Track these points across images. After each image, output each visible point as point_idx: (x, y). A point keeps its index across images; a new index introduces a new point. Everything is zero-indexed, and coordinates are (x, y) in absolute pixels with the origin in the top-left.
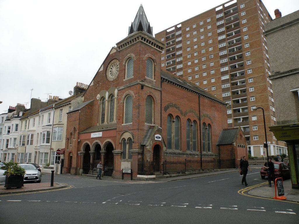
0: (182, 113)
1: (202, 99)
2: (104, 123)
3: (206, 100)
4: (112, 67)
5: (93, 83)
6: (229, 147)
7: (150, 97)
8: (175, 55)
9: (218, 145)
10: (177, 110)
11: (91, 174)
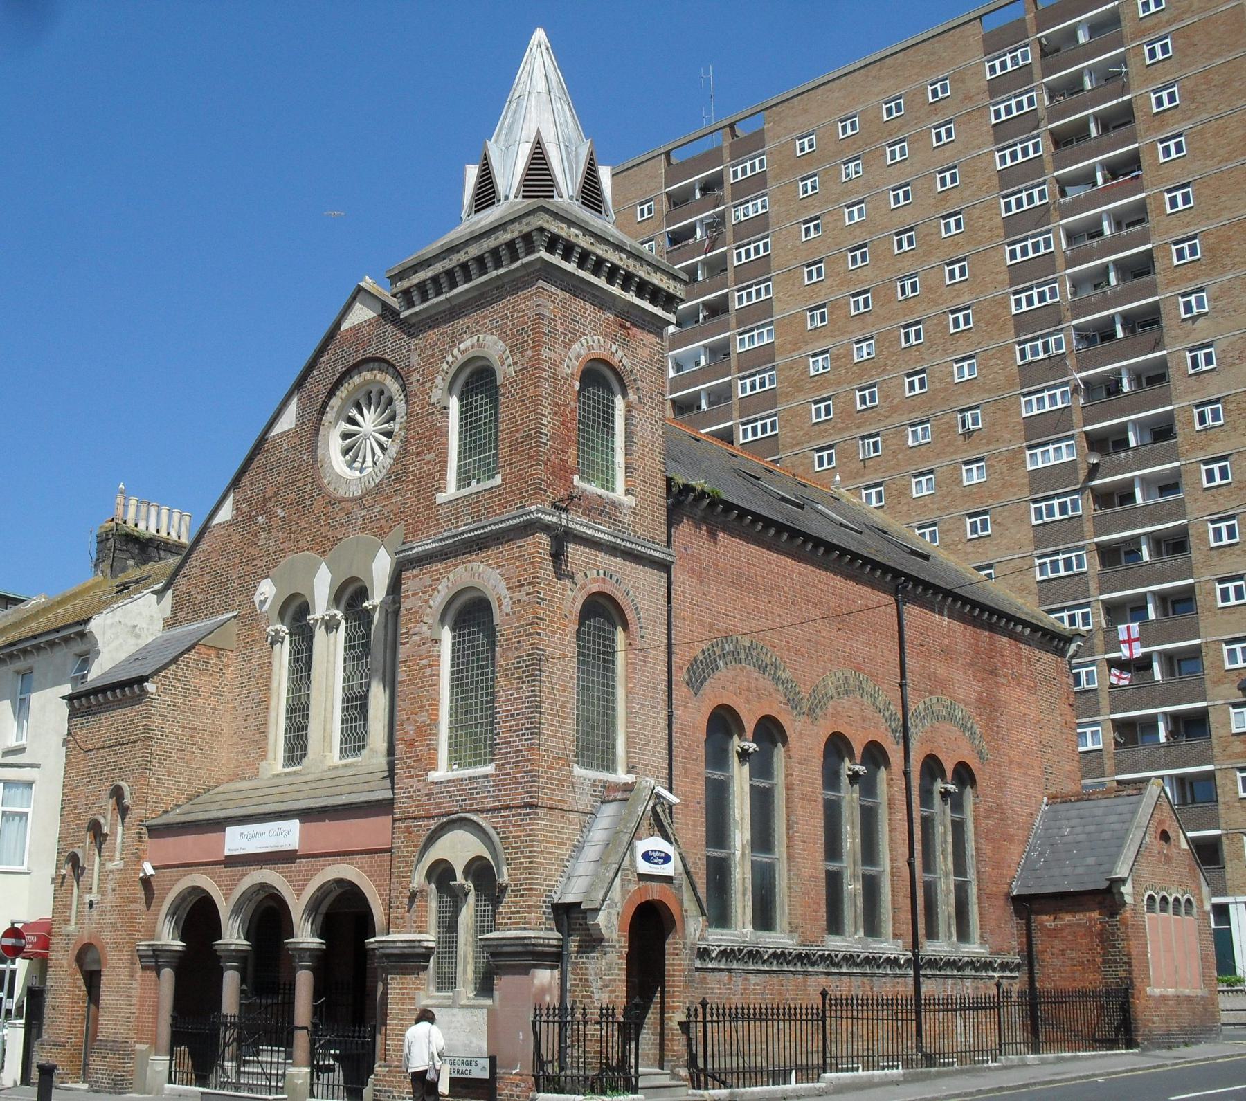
0: (793, 702)
2: (305, 761)
3: (942, 623)
4: (354, 413)
5: (229, 504)
7: (602, 611)
8: (726, 311)
10: (766, 682)
11: (224, 1085)
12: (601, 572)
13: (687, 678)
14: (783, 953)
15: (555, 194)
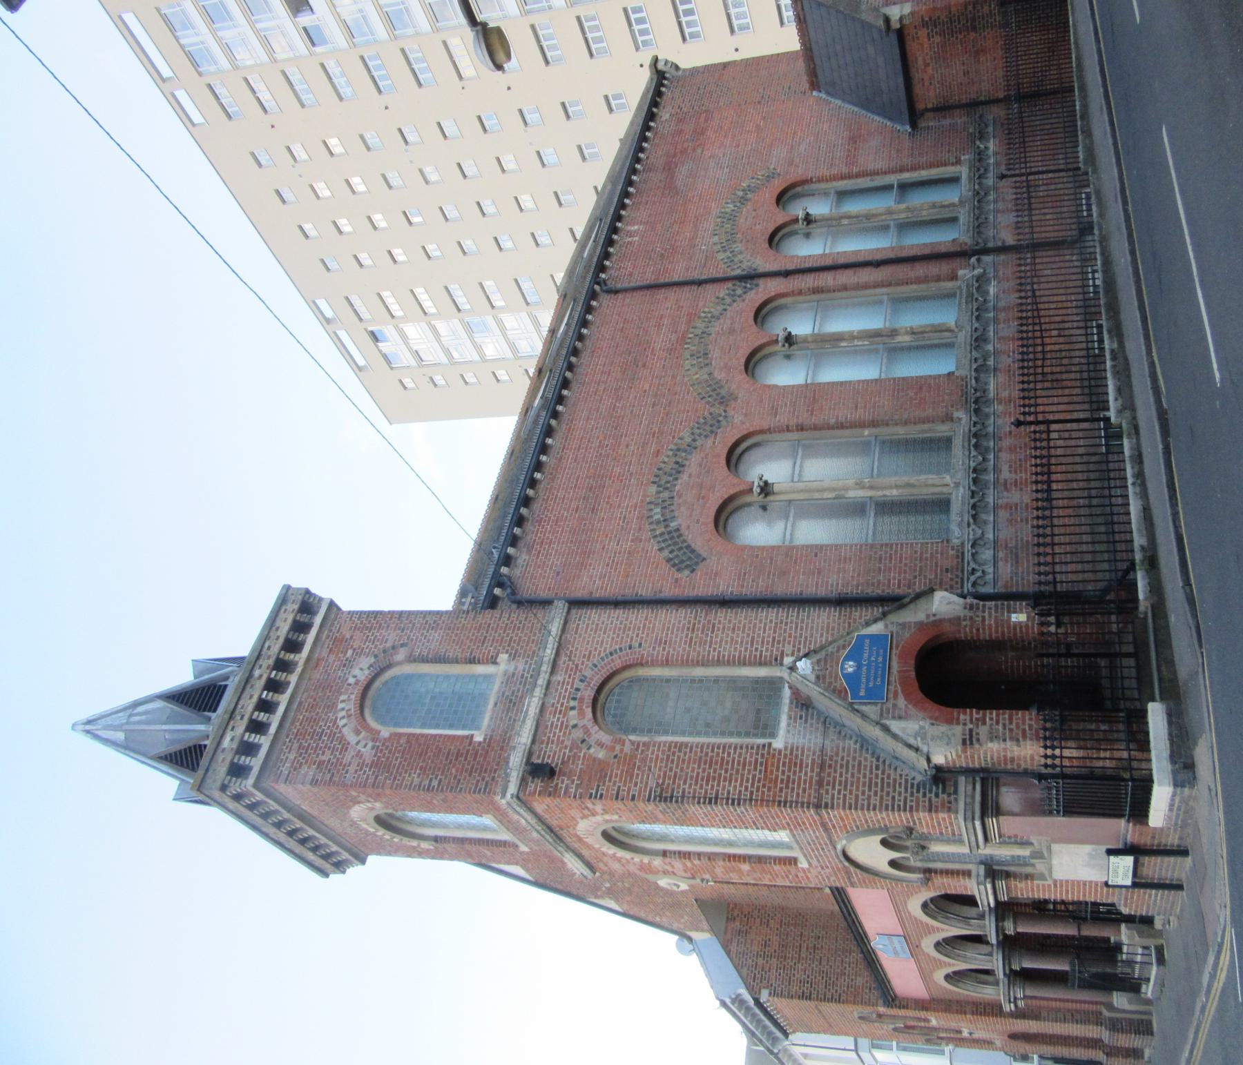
1: (621, 270)
6: (923, 49)
9: (914, 117)
12: (572, 703)
13: (687, 572)
14: (975, 435)
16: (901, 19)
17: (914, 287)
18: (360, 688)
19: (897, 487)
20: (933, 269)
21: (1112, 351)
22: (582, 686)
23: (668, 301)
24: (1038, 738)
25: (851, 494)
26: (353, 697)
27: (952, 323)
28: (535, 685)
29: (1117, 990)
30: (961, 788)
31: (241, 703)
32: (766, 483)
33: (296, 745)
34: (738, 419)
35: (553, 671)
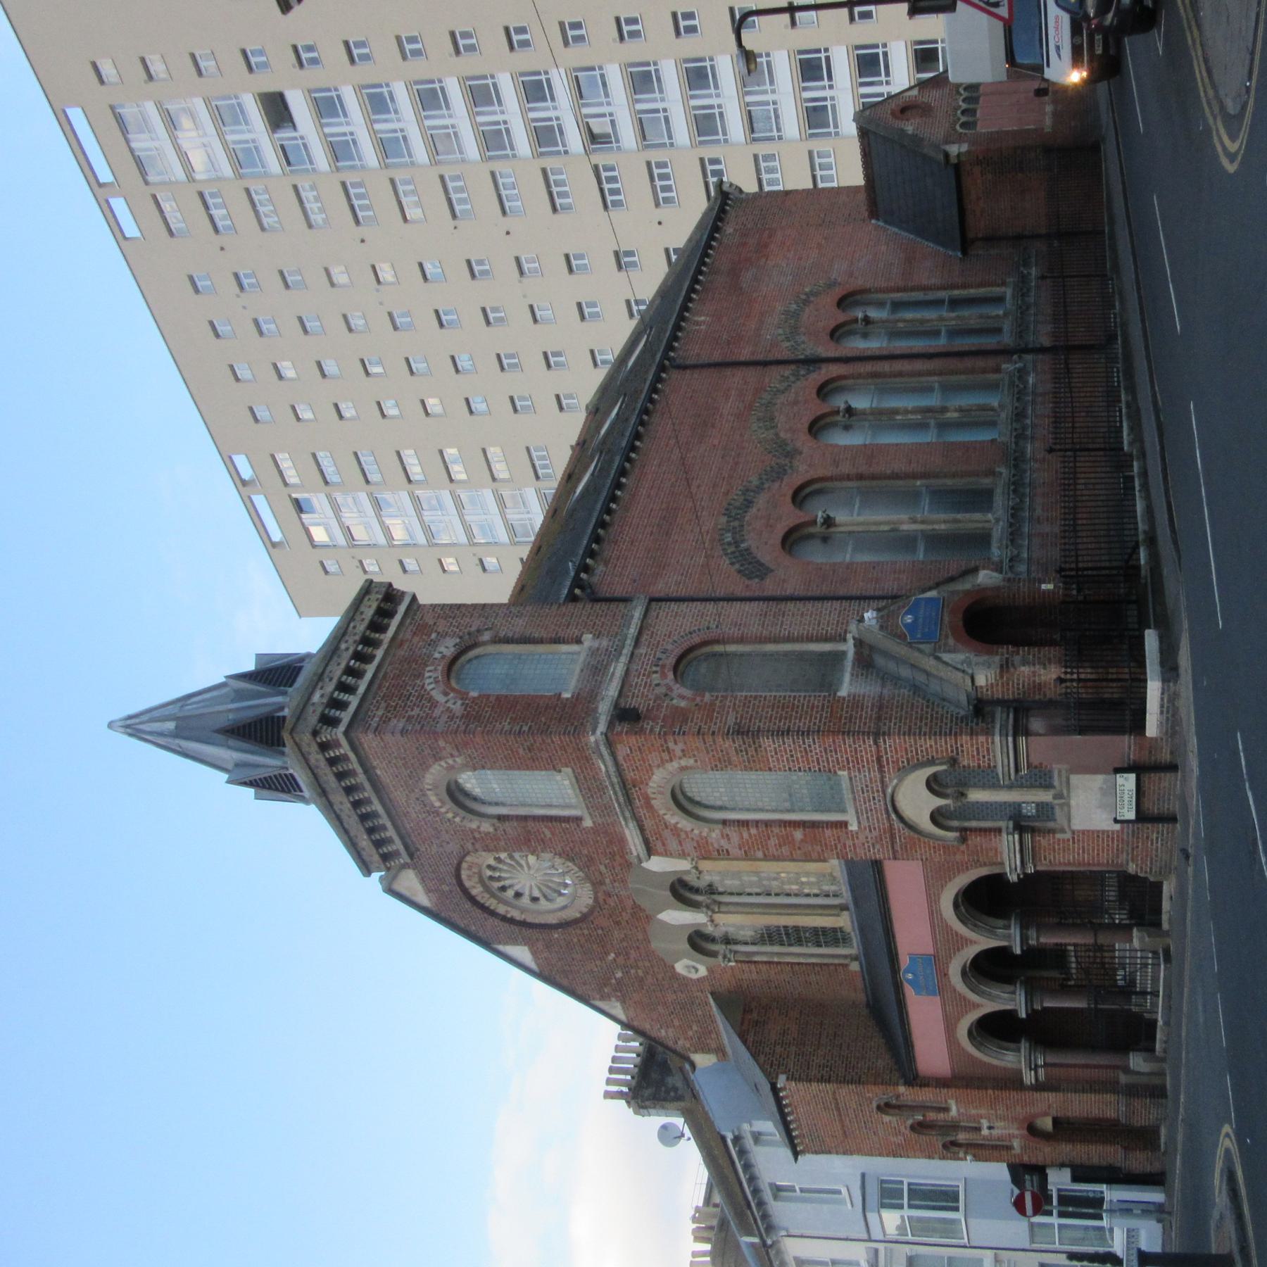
0: (778, 473)
1: (690, 350)
9: (965, 245)
10: (761, 501)
12: (654, 669)
14: (1014, 483)
15: (281, 714)
16: (959, 155)
17: (963, 377)
18: (446, 661)
19: (945, 522)
20: (980, 363)
21: (1127, 403)
22: (663, 656)
23: (735, 378)
24: (1060, 662)
25: (905, 527)
26: (440, 668)
27: (996, 404)
28: (620, 654)
29: (1134, 1050)
30: (998, 715)
31: (329, 668)
32: (828, 517)
33: (383, 705)
34: (802, 468)
35: (637, 643)
